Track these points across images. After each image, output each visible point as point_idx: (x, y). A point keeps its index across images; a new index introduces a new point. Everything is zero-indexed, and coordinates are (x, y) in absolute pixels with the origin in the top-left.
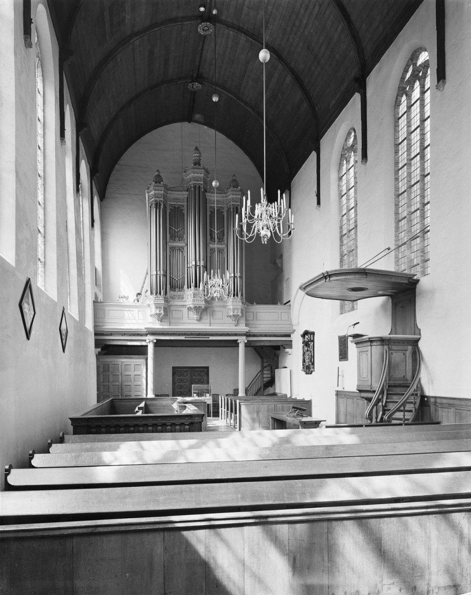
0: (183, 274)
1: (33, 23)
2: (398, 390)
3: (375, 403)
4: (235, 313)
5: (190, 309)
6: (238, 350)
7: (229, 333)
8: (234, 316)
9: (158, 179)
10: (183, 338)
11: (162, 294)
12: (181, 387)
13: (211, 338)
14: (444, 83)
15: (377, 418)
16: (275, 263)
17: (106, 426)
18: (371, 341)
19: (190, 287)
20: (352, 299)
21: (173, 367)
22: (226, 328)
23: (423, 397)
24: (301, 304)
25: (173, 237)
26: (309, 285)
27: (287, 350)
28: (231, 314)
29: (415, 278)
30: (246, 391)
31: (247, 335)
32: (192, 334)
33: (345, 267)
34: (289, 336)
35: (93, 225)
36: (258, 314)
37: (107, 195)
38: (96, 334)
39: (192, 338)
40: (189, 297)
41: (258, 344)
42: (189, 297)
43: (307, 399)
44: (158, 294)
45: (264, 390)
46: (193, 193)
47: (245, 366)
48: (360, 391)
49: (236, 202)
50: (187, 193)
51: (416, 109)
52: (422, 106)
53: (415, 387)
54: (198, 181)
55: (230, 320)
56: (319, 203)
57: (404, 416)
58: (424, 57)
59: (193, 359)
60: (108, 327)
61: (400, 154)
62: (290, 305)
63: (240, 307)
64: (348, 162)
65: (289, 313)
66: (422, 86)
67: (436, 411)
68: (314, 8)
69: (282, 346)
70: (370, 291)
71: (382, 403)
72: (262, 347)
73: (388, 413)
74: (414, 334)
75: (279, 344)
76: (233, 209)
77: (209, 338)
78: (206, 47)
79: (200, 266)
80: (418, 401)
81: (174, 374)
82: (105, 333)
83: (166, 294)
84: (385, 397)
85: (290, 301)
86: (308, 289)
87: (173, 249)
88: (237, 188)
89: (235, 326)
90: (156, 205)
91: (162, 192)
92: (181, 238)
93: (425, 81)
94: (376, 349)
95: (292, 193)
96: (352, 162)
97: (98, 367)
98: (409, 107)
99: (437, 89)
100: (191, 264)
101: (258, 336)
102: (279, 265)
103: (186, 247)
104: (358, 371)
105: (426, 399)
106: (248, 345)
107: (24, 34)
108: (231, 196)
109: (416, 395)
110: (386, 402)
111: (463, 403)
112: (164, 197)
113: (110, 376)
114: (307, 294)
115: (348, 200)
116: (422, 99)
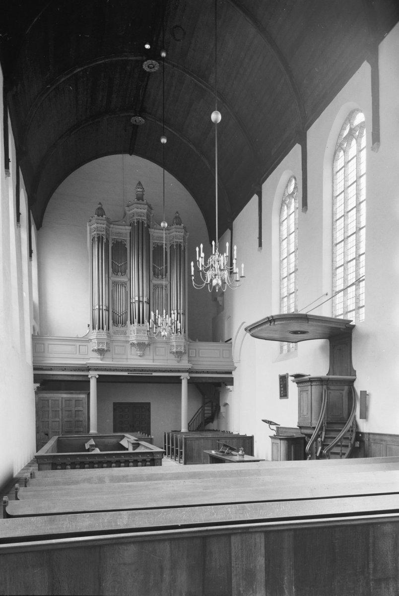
0: (126, 309)
2: (336, 427)
3: (315, 439)
4: (178, 350)
5: (133, 345)
6: (181, 386)
8: (177, 352)
9: (100, 212)
10: (126, 374)
11: (105, 329)
13: (154, 374)
14: (379, 145)
15: (316, 453)
17: (62, 463)
18: (311, 381)
19: (133, 323)
21: (115, 404)
23: (358, 433)
25: (116, 272)
26: (254, 328)
27: (229, 387)
28: (174, 350)
30: (189, 426)
31: (189, 371)
32: (135, 370)
33: (285, 311)
34: (231, 373)
35: (30, 256)
36: (200, 351)
38: (35, 369)
39: (148, 374)
40: (134, 333)
42: (132, 332)
43: (249, 435)
44: (101, 330)
46: (136, 229)
47: (188, 402)
49: (179, 239)
50: (130, 228)
51: (352, 165)
52: (358, 164)
53: (351, 424)
55: (172, 357)
56: (260, 245)
58: (360, 118)
59: (136, 396)
60: (49, 362)
61: (338, 206)
62: (231, 343)
63: (183, 344)
64: (288, 208)
65: (230, 351)
66: (359, 144)
69: (224, 383)
71: (321, 438)
73: (327, 448)
74: (351, 375)
75: (220, 381)
76: (177, 245)
80: (354, 435)
81: (115, 410)
82: (44, 368)
83: (109, 329)
84: (324, 433)
85: (231, 339)
86: (252, 332)
87: (115, 284)
88: (180, 225)
90: (99, 238)
92: (124, 272)
93: (361, 140)
94: (315, 390)
95: (233, 232)
96: (292, 208)
99: (372, 150)
100: (134, 299)
102: (221, 303)
103: (129, 282)
105: (360, 435)
106: (191, 382)
109: (352, 431)
110: (325, 437)
112: (107, 230)
113: (50, 411)
114: (252, 335)
115: (288, 244)
116: (357, 156)
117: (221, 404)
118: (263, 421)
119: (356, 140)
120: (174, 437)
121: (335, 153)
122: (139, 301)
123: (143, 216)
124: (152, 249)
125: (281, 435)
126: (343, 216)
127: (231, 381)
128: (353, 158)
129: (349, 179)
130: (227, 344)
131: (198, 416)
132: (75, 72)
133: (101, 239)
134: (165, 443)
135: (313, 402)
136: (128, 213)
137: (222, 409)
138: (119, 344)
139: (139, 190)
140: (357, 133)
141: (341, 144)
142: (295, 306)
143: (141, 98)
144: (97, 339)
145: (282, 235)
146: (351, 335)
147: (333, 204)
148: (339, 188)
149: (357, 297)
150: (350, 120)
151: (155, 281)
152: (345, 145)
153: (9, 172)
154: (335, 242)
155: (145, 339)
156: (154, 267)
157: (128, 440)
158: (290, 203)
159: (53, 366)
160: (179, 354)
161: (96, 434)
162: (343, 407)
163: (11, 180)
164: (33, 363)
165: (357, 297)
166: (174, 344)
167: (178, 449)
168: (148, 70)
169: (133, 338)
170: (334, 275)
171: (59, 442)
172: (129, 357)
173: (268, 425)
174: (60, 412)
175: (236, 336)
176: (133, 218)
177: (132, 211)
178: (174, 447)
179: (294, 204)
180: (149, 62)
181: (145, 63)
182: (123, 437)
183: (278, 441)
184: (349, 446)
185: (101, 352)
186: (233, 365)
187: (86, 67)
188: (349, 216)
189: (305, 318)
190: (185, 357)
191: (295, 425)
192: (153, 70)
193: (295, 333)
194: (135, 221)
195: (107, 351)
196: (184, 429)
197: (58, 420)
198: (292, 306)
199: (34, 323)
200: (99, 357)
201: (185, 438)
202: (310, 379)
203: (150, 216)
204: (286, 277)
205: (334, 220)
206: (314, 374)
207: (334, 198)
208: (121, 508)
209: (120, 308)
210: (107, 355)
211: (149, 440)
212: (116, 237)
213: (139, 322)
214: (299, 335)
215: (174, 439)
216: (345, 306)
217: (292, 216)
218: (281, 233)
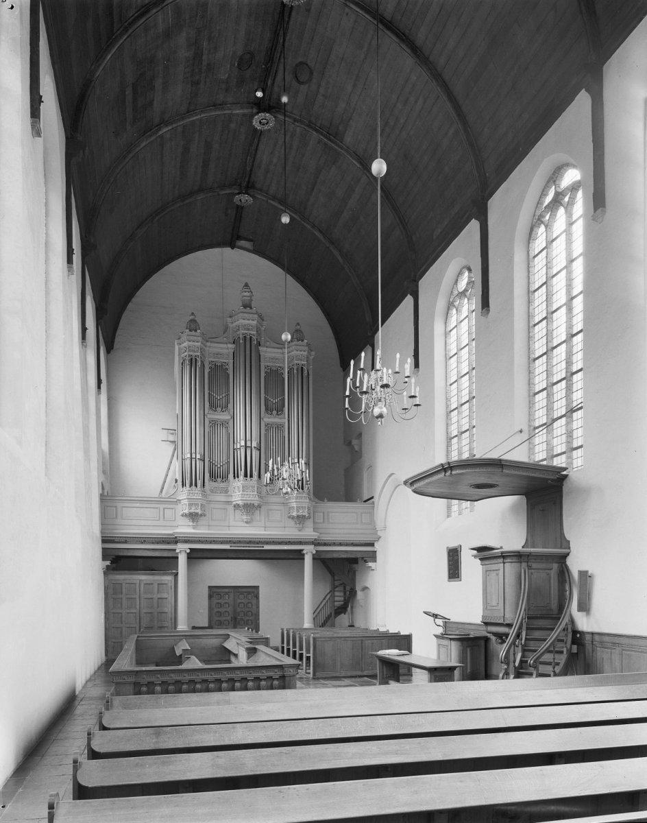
0: (228, 457)
1: (43, 102)
2: (541, 623)
4: (300, 514)
5: (237, 507)
7: (241, 540)
8: (298, 516)
9: (193, 325)
10: (227, 547)
11: (199, 485)
12: (220, 614)
13: (267, 547)
14: (604, 212)
16: (349, 444)
18: (504, 556)
19: (238, 477)
20: (473, 498)
22: (202, 532)
23: (575, 632)
24: (389, 502)
25: (213, 406)
26: (419, 479)
27: (370, 564)
28: (295, 514)
29: (564, 473)
31: (316, 543)
32: (240, 542)
33: (454, 457)
34: (372, 545)
35: (99, 387)
36: (330, 514)
37: (116, 346)
38: (104, 541)
40: (239, 491)
41: (329, 556)
44: (193, 486)
45: (335, 618)
46: (242, 346)
48: (486, 624)
50: (233, 346)
52: (569, 242)
54: (248, 330)
55: (292, 523)
57: (554, 659)
58: (571, 176)
62: (373, 503)
65: (372, 514)
66: (569, 214)
67: (593, 651)
68: (416, 102)
70: (499, 488)
72: (333, 559)
74: (561, 548)
77: (263, 547)
78: (261, 147)
79: (251, 447)
80: (570, 636)
81: (210, 597)
82: (117, 540)
85: (372, 498)
87: (214, 423)
88: (303, 341)
89: (300, 531)
91: (199, 344)
92: (225, 408)
94: (510, 568)
97: (106, 588)
98: (550, 242)
99: (593, 220)
101: (330, 545)
102: (356, 448)
103: (231, 422)
104: (483, 599)
105: (578, 636)
106: (319, 559)
107: (31, 117)
108: (295, 352)
110: (526, 639)
111: (634, 642)
113: (124, 599)
114: (415, 491)
116: (568, 232)
117: (358, 588)
118: (425, 613)
119: (566, 208)
120: (297, 636)
121: (532, 230)
122: (246, 447)
123: (252, 330)
124: (263, 375)
125: (450, 633)
126: (545, 318)
127: (373, 556)
128: (561, 234)
129: (554, 264)
130: (365, 505)
131: (325, 605)
132: (160, 133)
133: (194, 363)
134: (283, 643)
135: (507, 586)
136: (230, 325)
137: (360, 595)
138: (217, 506)
139: (245, 294)
140: (566, 199)
141: (541, 216)
142: (471, 449)
143: (248, 169)
144: (188, 499)
145: (450, 350)
146: (562, 488)
147: (529, 302)
148: (539, 278)
149: (569, 434)
150: (555, 181)
151: (268, 419)
152: (547, 218)
153: (72, 268)
154: (533, 356)
155: (253, 498)
156: (266, 400)
157: (237, 642)
158: (461, 305)
159: (128, 537)
160: (300, 519)
161: (185, 631)
162: (550, 594)
163: (76, 279)
164: (102, 532)
165: (569, 434)
166: (294, 505)
167: (304, 652)
168: (259, 127)
169: (237, 497)
170: (531, 404)
171: (139, 647)
172: (231, 524)
173: (432, 618)
174: (138, 600)
175: (382, 491)
176: (238, 333)
177: (234, 324)
178: (297, 649)
179: (468, 306)
180: (262, 115)
181: (256, 117)
182: (228, 636)
183: (446, 642)
184: (565, 653)
185: (193, 517)
186: (377, 534)
187: (174, 125)
188: (554, 318)
189: (498, 464)
190: (309, 523)
191: (477, 618)
192: (266, 127)
193: (479, 486)
194: (241, 336)
195: (201, 515)
196: (307, 624)
197: (134, 611)
198: (466, 448)
199: (102, 478)
200: (191, 524)
201: (314, 639)
202: (502, 553)
203: (260, 329)
204: (455, 409)
205: (531, 325)
206: (508, 547)
207: (530, 293)
208: (227, 742)
209: (220, 459)
210: (202, 521)
211: (264, 640)
212: (214, 360)
213: (246, 475)
214: (484, 489)
215: (291, 635)
216: (550, 448)
217: (465, 325)
218: (448, 348)
